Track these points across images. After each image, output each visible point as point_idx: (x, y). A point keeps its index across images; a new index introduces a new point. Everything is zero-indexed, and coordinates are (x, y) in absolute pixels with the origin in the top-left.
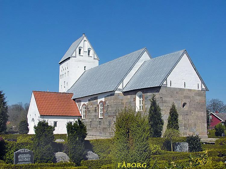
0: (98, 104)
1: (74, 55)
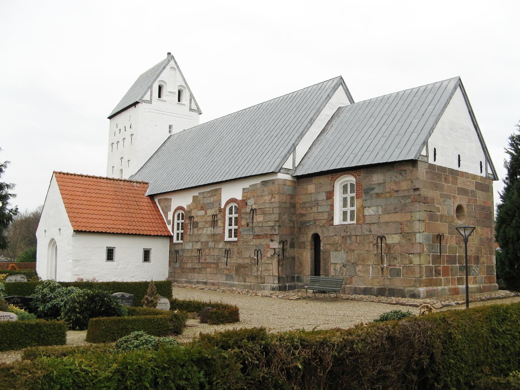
0: (222, 207)
1: (147, 97)
